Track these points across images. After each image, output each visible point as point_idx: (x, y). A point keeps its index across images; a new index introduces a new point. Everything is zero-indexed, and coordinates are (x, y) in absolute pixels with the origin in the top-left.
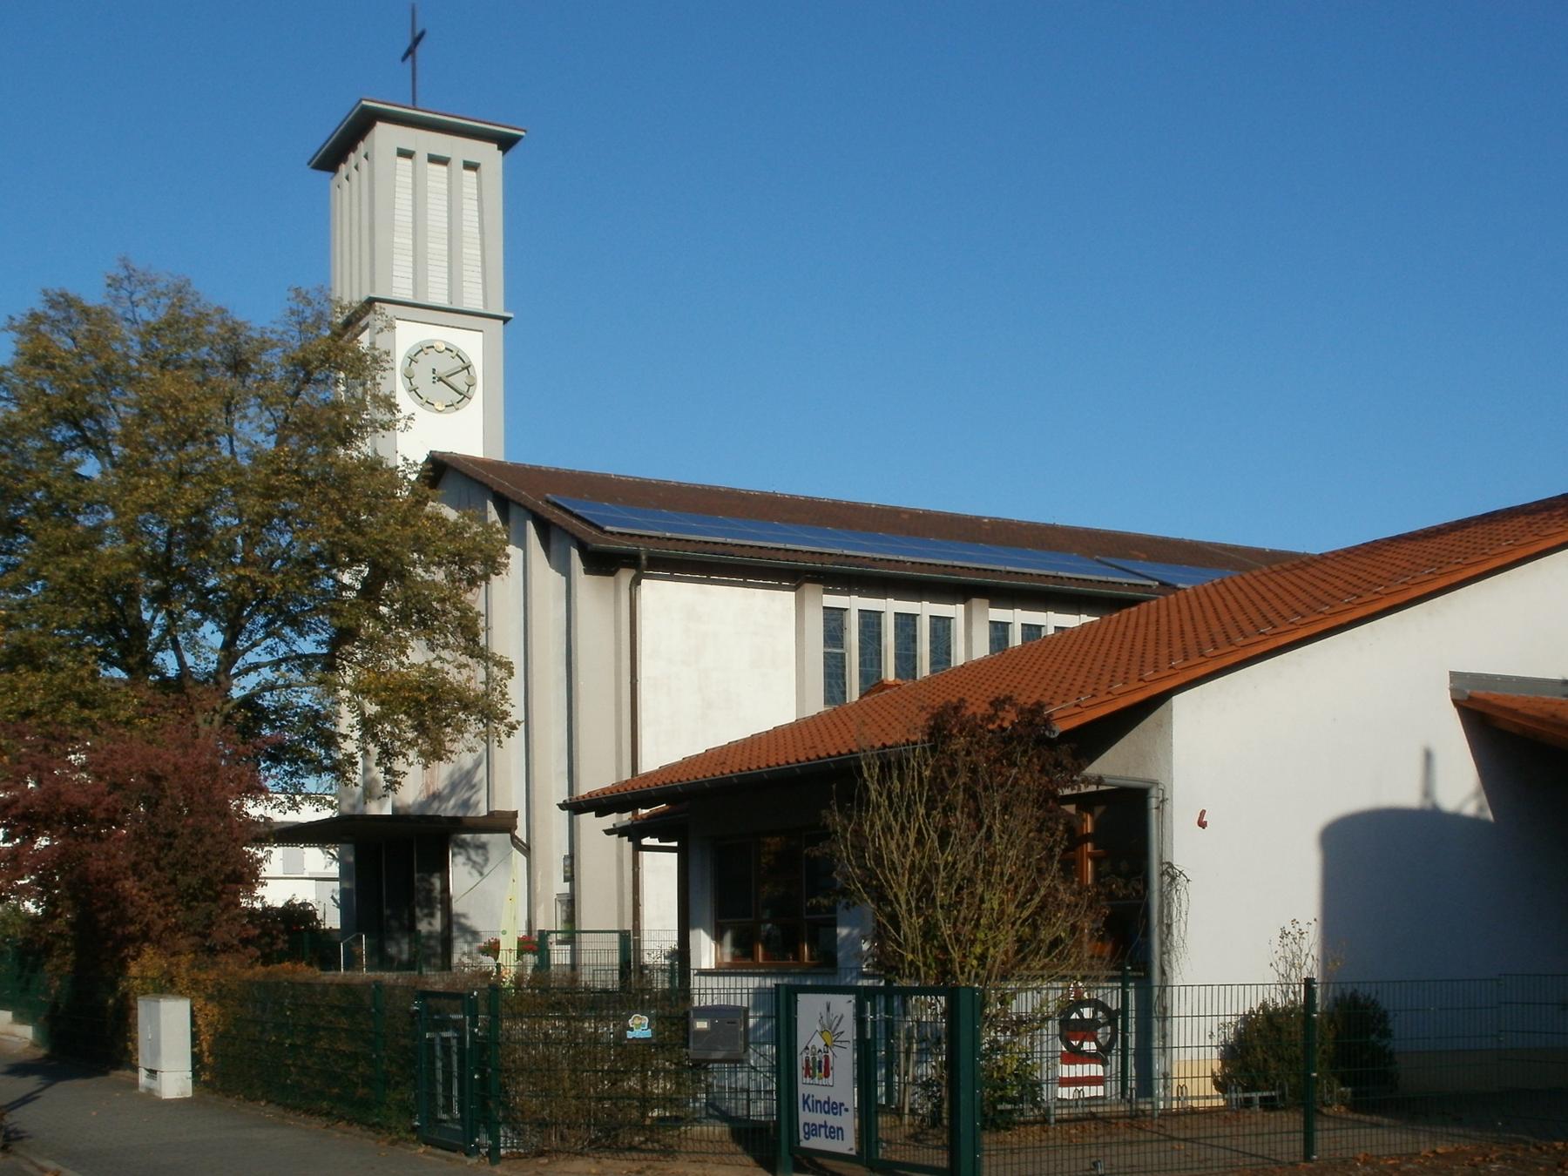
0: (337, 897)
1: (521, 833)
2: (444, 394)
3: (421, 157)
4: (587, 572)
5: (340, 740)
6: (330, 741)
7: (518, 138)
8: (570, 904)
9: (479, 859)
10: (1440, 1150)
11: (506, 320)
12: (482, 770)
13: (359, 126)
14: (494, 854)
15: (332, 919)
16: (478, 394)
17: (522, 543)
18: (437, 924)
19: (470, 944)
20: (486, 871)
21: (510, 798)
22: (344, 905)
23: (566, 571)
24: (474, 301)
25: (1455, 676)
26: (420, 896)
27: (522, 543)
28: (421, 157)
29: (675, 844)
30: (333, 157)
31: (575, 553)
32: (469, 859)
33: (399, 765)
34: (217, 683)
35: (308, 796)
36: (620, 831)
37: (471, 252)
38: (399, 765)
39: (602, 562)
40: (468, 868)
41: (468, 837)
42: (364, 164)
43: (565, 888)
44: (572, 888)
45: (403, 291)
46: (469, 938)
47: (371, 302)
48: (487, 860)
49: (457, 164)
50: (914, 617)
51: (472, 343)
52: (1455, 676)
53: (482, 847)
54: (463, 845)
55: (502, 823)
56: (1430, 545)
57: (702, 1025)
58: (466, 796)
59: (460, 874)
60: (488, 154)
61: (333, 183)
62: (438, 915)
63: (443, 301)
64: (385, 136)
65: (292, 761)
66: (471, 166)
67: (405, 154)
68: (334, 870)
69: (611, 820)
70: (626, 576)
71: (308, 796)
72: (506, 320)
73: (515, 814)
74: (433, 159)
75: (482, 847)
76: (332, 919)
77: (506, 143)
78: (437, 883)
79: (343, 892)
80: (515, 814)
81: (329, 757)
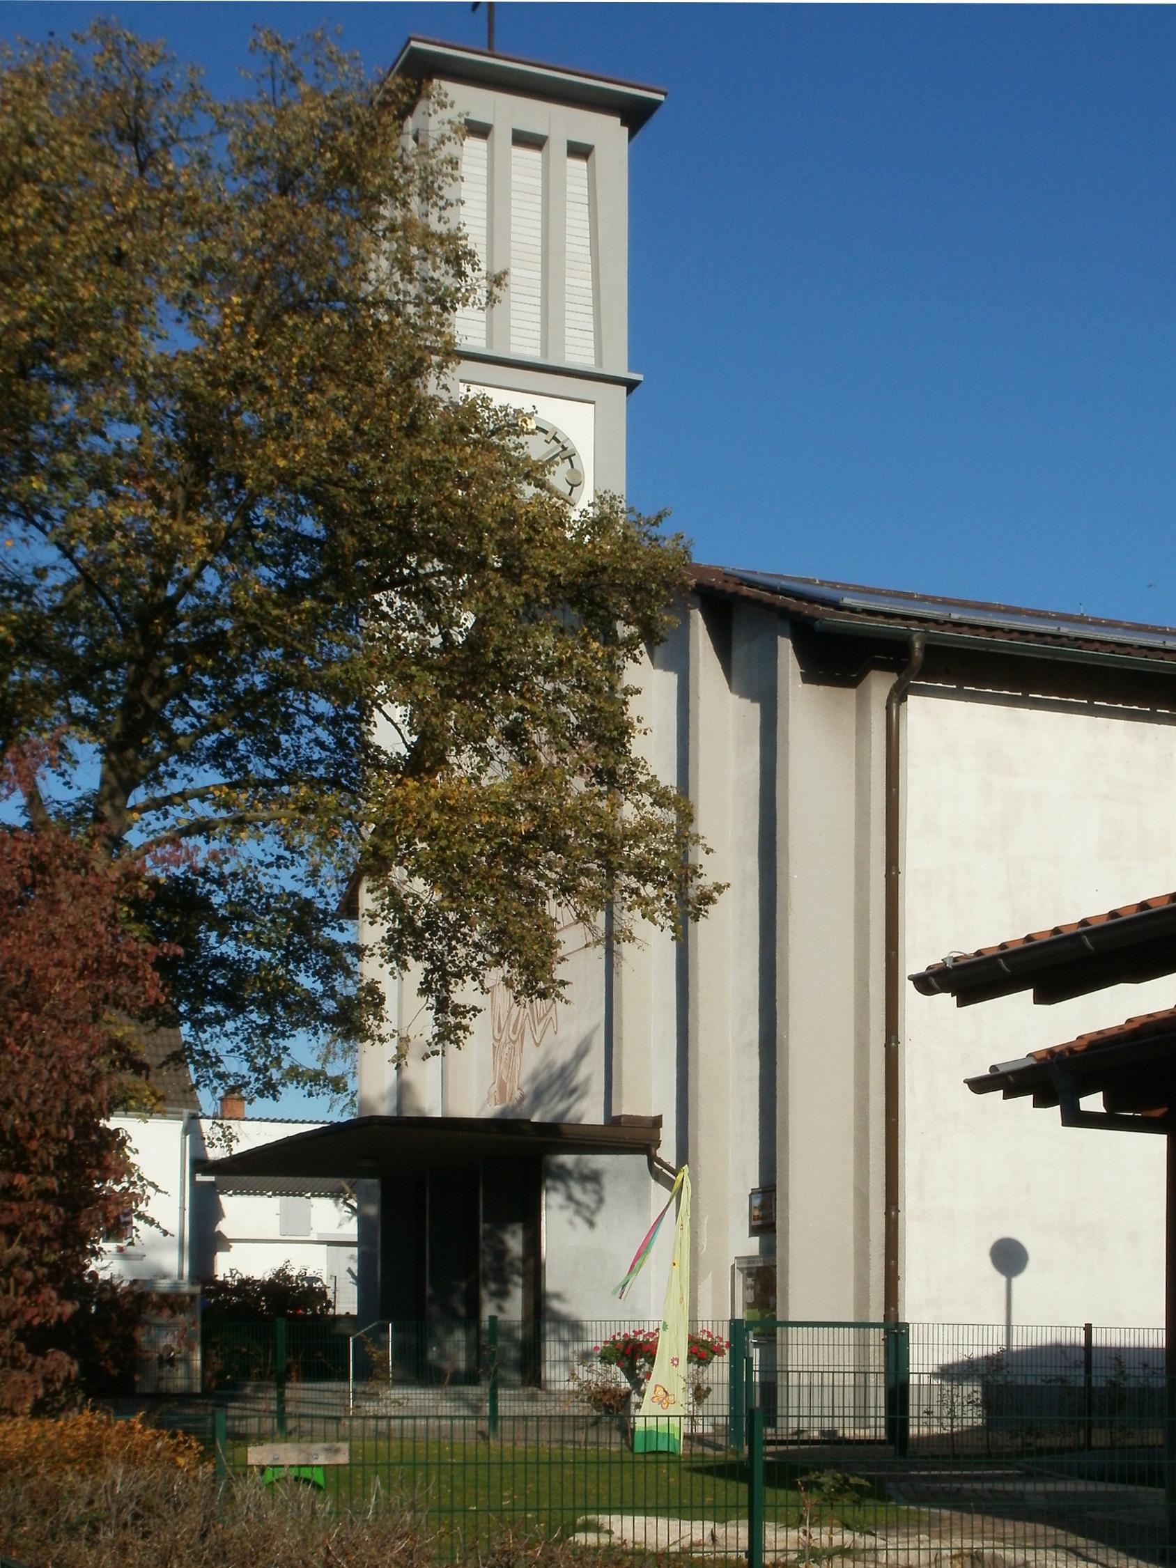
0: (355, 1268)
1: (667, 1151)
3: (502, 135)
4: (806, 678)
5: (350, 959)
6: (337, 960)
8: (764, 1279)
9: (587, 1199)
11: (631, 386)
12: (593, 1067)
14: (611, 1188)
15: (346, 1302)
17: (680, 663)
18: (514, 1309)
19: (566, 1344)
20: (599, 1219)
21: (649, 1093)
22: (363, 1280)
23: (764, 694)
24: (580, 354)
26: (486, 1261)
27: (680, 663)
28: (502, 135)
29: (1158, 1113)
31: (786, 647)
32: (570, 1198)
33: (464, 993)
34: (99, 818)
35: (295, 1074)
37: (578, 282)
38: (464, 993)
40: (568, 1214)
41: (568, 1160)
43: (752, 1246)
44: (769, 1249)
46: (565, 1335)
48: (601, 1201)
49: (557, 147)
53: (593, 1178)
54: (563, 1175)
55: (632, 1137)
58: (561, 1107)
59: (556, 1218)
60: (606, 132)
62: (517, 1294)
63: (531, 353)
65: (266, 1005)
66: (579, 151)
68: (351, 1230)
70: (879, 685)
71: (295, 1074)
72: (631, 386)
73: (657, 1122)
75: (593, 1178)
76: (346, 1302)
77: (635, 115)
78: (515, 1244)
79: (363, 1260)
80: (657, 1122)
81: (331, 994)
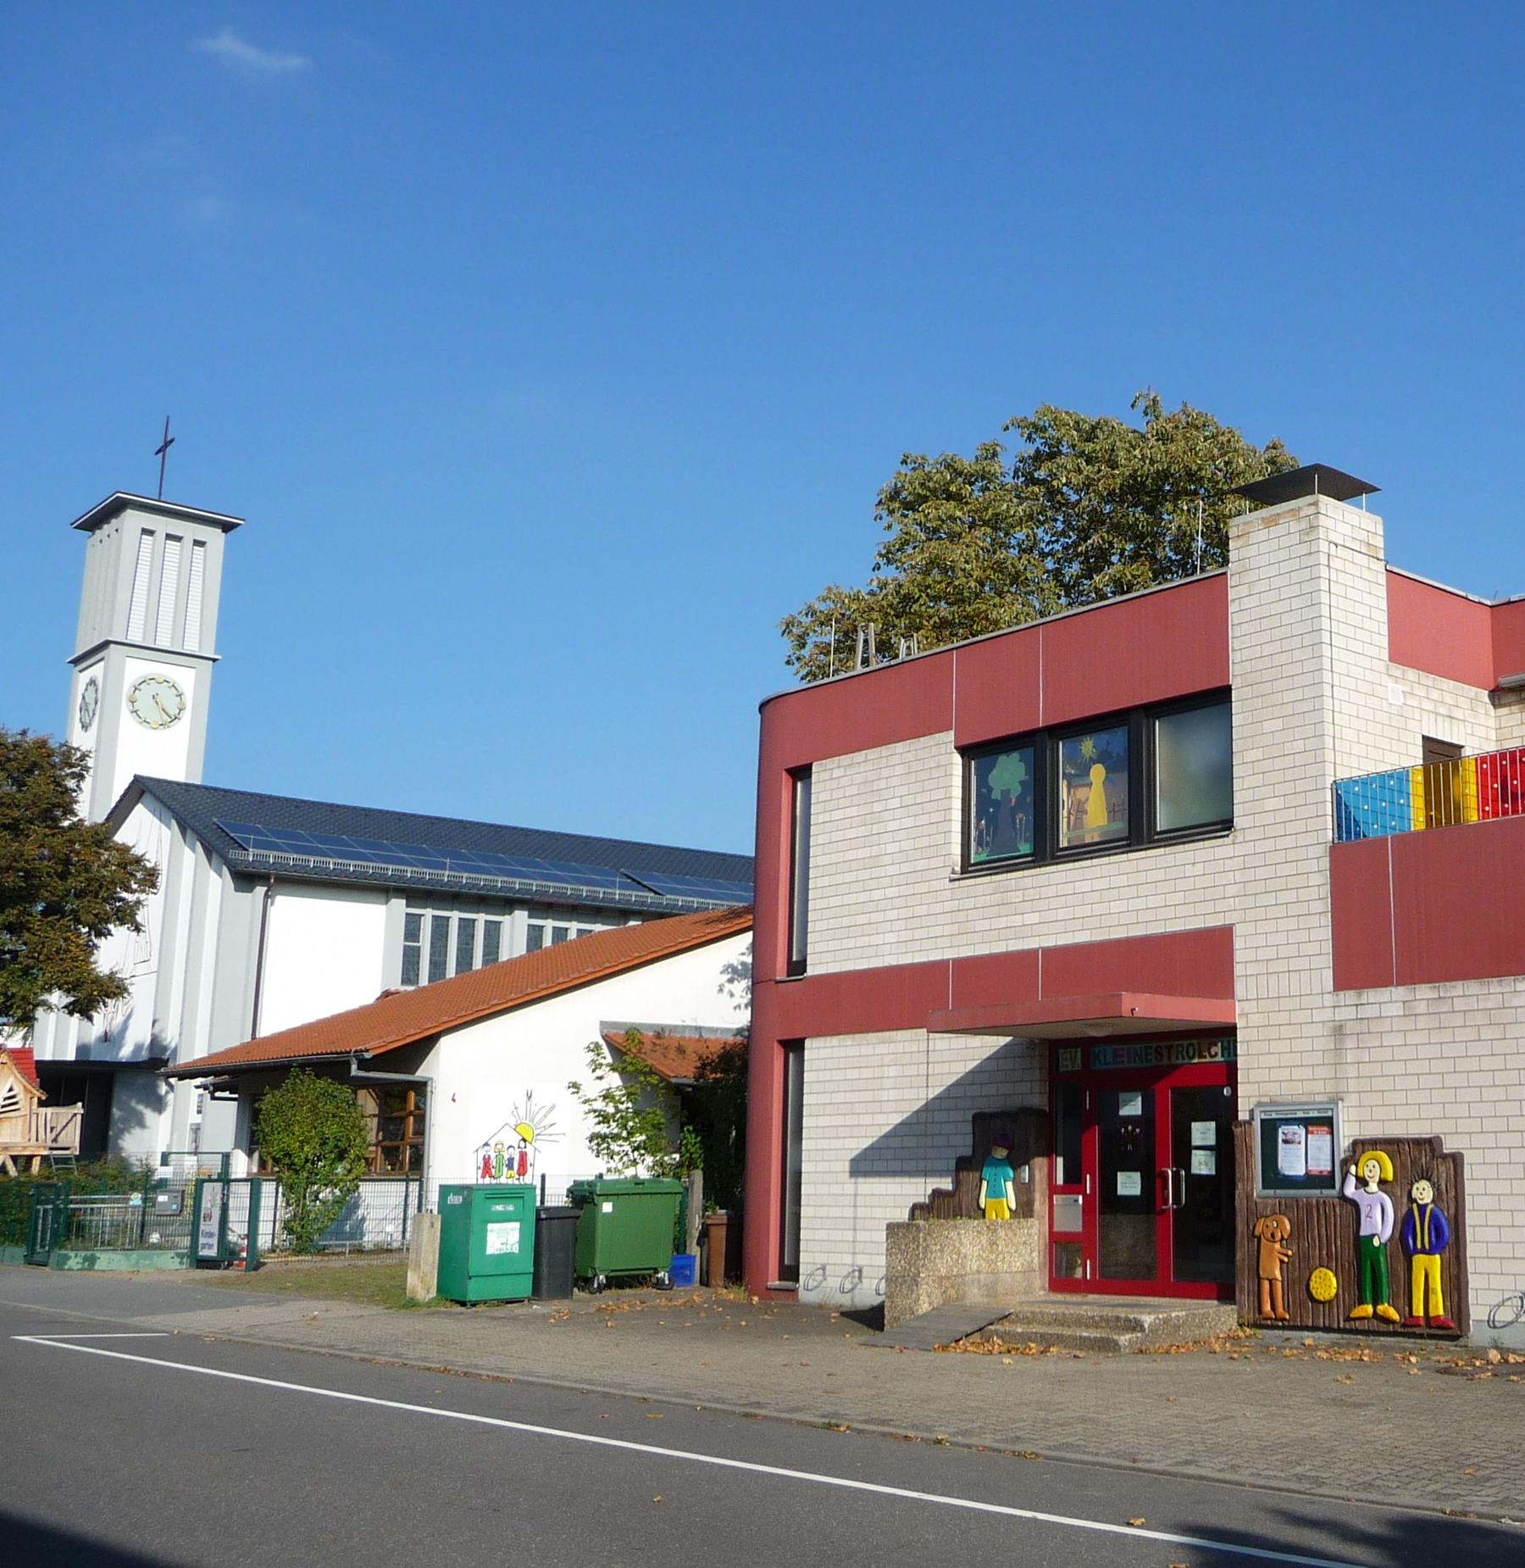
2: (155, 715)
7: (238, 525)
10: (1307, 1342)
11: (214, 660)
13: (115, 509)
16: (186, 716)
24: (191, 646)
25: (602, 1023)
28: (160, 535)
30: (93, 523)
36: (205, 1088)
39: (245, 879)
42: (114, 535)
45: (135, 637)
47: (105, 645)
50: (448, 918)
51: (187, 678)
52: (602, 1023)
56: (531, 992)
57: (607, 1207)
60: (214, 536)
61: (91, 541)
64: (132, 520)
66: (198, 543)
67: (145, 532)
69: (199, 1081)
70: (260, 890)
74: (169, 537)
77: (227, 527)
